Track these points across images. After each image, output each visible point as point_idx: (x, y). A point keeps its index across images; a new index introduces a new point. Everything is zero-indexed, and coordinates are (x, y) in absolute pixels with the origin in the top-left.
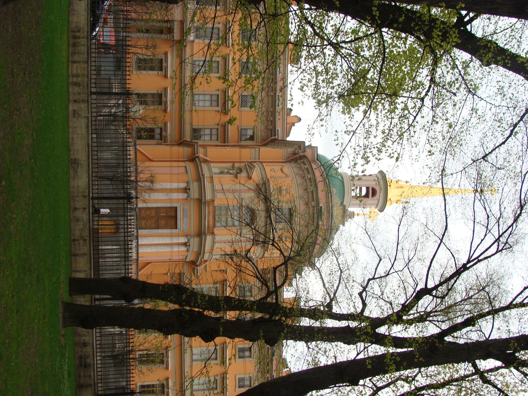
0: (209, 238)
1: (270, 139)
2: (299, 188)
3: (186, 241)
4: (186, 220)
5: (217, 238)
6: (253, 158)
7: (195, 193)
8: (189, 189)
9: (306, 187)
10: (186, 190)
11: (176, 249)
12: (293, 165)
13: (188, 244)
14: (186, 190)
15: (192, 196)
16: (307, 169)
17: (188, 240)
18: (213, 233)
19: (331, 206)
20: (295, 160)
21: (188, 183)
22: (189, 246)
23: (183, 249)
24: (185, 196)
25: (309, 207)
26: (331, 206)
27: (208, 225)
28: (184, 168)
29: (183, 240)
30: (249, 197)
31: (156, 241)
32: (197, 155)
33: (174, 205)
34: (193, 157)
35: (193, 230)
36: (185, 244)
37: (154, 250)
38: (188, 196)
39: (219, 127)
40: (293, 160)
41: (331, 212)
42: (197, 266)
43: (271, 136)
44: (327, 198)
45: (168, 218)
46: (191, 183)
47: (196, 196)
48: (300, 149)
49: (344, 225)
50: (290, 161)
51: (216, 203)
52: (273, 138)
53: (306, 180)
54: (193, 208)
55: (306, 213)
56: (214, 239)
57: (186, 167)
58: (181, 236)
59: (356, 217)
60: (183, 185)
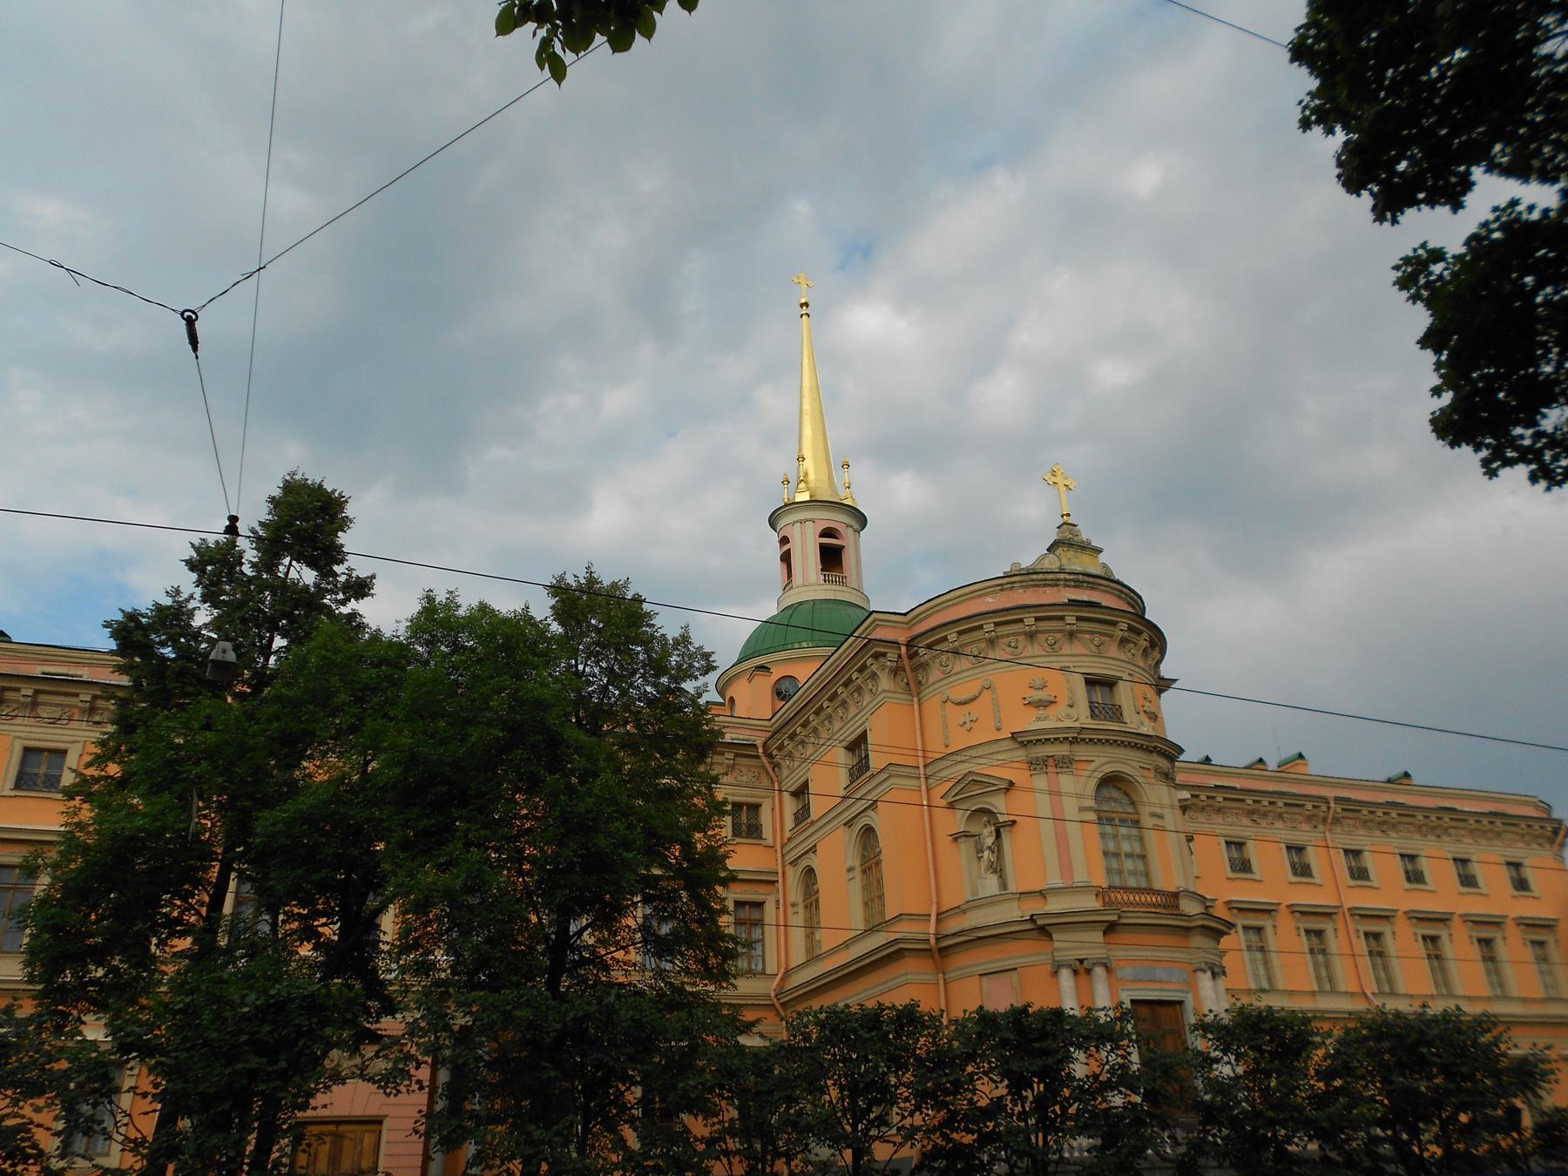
6: (914, 782)
8: (1081, 961)
10: (1082, 969)
12: (935, 674)
15: (1099, 953)
18: (1176, 895)
28: (985, 979)
32: (933, 941)
46: (1059, 956)
48: (884, 655)
49: (1099, 551)
60: (1066, 976)
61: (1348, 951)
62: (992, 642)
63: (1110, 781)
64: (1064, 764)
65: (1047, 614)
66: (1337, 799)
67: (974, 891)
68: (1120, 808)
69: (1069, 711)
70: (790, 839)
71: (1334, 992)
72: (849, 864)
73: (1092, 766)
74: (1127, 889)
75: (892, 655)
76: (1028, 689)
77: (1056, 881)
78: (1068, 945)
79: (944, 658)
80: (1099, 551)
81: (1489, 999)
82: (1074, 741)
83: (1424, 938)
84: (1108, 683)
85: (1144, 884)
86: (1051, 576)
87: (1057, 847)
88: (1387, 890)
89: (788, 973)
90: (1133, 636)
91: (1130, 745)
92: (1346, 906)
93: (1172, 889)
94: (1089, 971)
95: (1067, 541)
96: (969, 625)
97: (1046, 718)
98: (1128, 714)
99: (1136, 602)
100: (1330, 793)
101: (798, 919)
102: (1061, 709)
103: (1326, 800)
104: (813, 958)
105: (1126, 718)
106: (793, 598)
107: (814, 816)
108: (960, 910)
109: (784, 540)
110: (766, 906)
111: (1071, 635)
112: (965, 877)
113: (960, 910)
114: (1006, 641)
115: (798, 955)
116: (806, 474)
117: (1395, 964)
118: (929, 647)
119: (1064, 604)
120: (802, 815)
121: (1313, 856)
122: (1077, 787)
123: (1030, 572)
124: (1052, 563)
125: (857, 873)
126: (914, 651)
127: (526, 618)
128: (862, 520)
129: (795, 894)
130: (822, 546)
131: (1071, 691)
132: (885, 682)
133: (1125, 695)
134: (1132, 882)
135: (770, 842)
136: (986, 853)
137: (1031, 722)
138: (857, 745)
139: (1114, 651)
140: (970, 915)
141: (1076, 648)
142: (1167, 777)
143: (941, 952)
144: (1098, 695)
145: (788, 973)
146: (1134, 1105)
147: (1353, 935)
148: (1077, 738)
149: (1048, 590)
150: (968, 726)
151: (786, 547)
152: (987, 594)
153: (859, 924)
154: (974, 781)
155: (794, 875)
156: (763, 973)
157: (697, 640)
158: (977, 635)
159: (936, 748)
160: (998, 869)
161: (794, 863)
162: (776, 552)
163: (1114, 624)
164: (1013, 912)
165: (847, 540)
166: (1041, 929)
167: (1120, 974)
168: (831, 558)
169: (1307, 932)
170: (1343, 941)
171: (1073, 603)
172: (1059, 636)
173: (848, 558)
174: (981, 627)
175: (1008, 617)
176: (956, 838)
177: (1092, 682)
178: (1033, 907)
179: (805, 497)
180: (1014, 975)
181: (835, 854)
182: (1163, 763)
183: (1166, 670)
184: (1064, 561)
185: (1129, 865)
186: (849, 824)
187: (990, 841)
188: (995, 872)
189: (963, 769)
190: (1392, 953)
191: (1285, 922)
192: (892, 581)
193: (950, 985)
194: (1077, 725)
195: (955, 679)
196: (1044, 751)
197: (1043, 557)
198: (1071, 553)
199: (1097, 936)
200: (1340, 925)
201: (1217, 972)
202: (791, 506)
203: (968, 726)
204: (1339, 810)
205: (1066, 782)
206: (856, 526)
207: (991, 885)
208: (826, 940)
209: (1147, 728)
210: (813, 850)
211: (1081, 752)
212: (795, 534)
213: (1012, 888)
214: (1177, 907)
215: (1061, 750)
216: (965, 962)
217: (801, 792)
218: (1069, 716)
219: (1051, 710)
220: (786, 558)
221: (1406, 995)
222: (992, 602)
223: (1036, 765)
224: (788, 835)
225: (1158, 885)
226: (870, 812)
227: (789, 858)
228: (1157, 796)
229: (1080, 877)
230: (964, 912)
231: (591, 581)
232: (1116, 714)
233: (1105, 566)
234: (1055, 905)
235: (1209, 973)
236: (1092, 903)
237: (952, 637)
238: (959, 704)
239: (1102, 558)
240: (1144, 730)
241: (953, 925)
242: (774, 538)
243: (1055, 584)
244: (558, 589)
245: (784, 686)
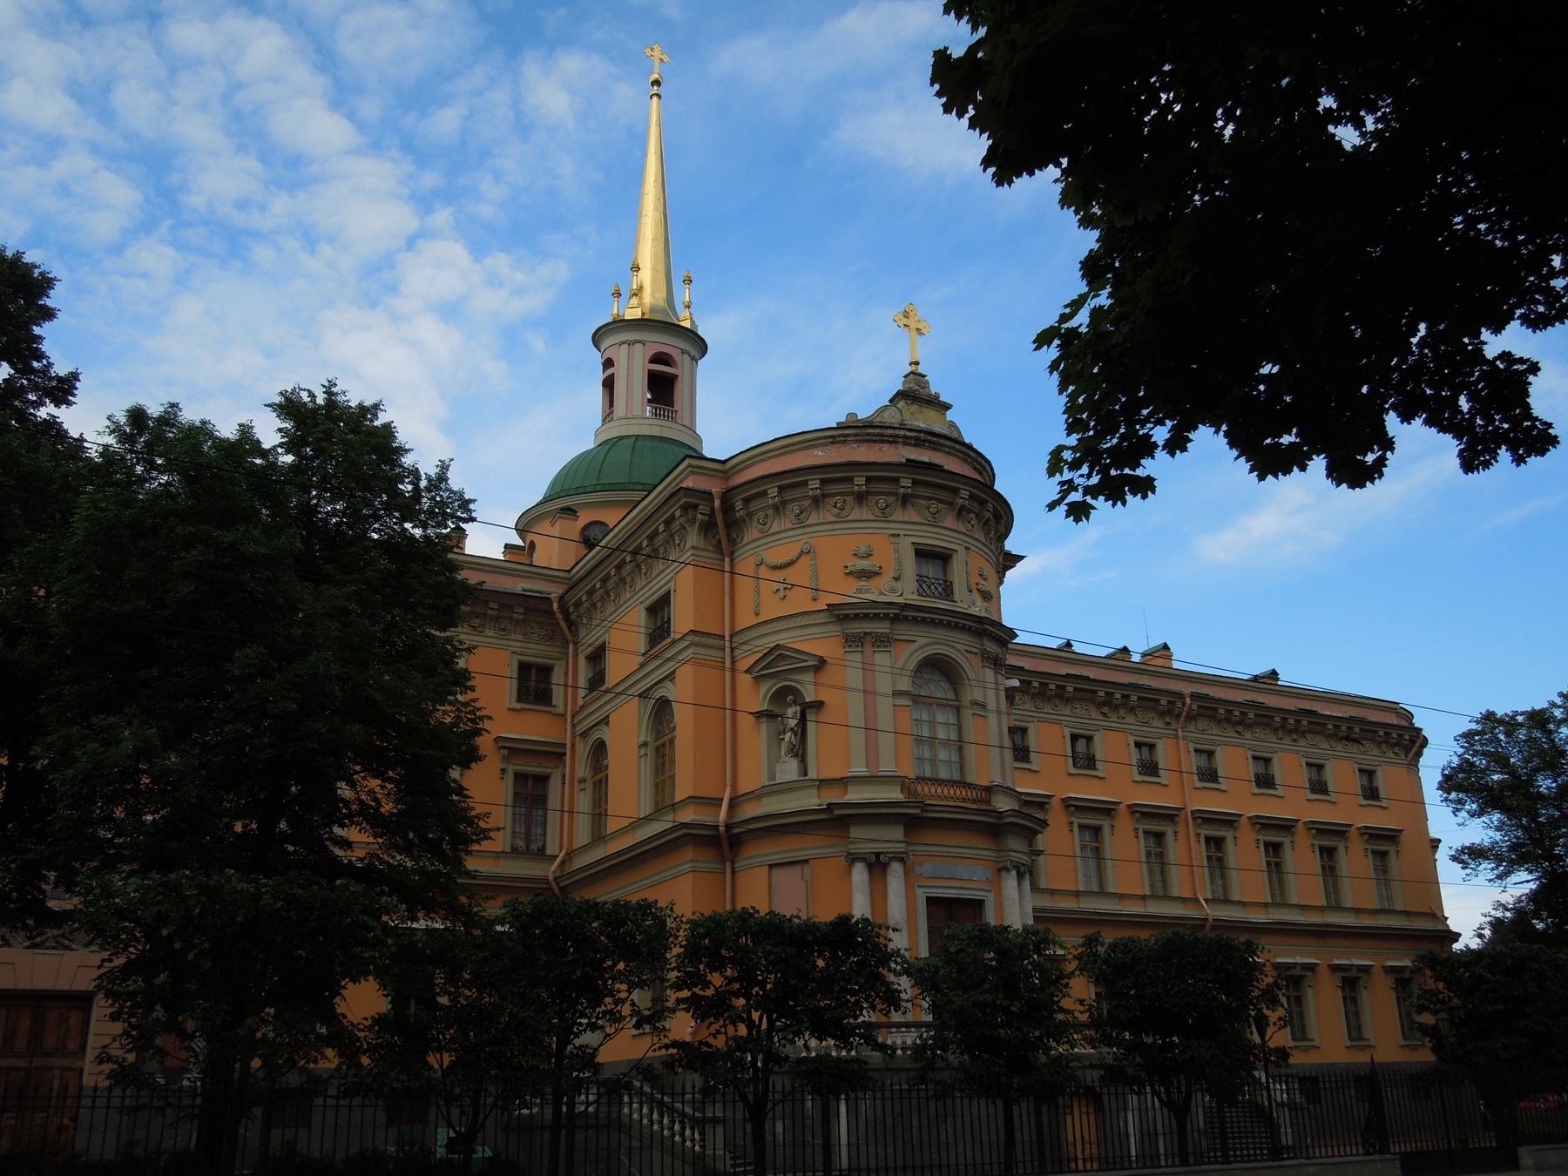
2: (773, 530)
6: (719, 653)
7: (889, 838)
8: (878, 855)
10: (877, 866)
12: (751, 533)
15: (901, 847)
16: (781, 489)
18: (989, 790)
21: (853, 859)
24: (896, 869)
25: (913, 496)
27: (974, 801)
28: (776, 873)
30: (892, 667)
32: (722, 829)
35: (978, 846)
39: (511, 768)
44: (882, 442)
47: (897, 832)
48: (695, 507)
49: (947, 407)
50: (733, 542)
51: (909, 771)
52: (555, 606)
55: (928, 508)
57: (771, 866)
58: (1000, 887)
59: (921, 369)
60: (859, 874)
61: (1186, 862)
63: (938, 666)
64: (883, 641)
65: (881, 476)
66: (1194, 696)
67: (772, 776)
68: (941, 690)
69: (894, 584)
70: (582, 707)
71: (1167, 897)
72: (642, 739)
73: (914, 646)
74: (937, 781)
75: (703, 508)
76: (868, 552)
77: (859, 769)
78: (866, 838)
80: (947, 407)
81: (1322, 909)
82: (895, 619)
83: (1321, 849)
84: (942, 558)
85: (956, 777)
86: (889, 432)
87: (869, 730)
88: (1235, 796)
89: (570, 855)
90: (976, 507)
91: (956, 627)
92: (1190, 809)
93: (986, 783)
94: (885, 866)
95: (915, 393)
96: (790, 482)
97: (868, 591)
98: (959, 591)
99: (982, 465)
100: (1187, 689)
101: (584, 802)
102: (884, 582)
103: (1181, 696)
104: (599, 837)
105: (957, 596)
106: (614, 431)
107: (610, 680)
108: (756, 795)
109: (608, 363)
110: (552, 780)
111: (905, 500)
112: (760, 762)
113: (756, 795)
114: (873, 499)
115: (583, 835)
116: (641, 288)
117: (1233, 875)
118: (747, 501)
119: (901, 464)
120: (597, 681)
121: (1163, 757)
122: (892, 667)
123: (868, 424)
124: (892, 417)
125: (650, 751)
126: (726, 506)
127: (246, 441)
128: (702, 347)
129: (582, 770)
130: (651, 374)
131: (899, 562)
132: (693, 538)
133: (958, 572)
134: (944, 774)
135: (560, 710)
136: (788, 736)
137: (850, 592)
138: (659, 608)
139: (950, 522)
140: (765, 801)
141: (910, 514)
142: (997, 663)
143: (725, 843)
144: (932, 570)
145: (570, 855)
146: (708, 966)
147: (1193, 838)
148: (902, 615)
149: (885, 447)
150: (782, 593)
151: (609, 372)
152: (816, 446)
153: (646, 809)
154: (777, 654)
155: (583, 750)
156: (542, 850)
157: (455, 482)
158: (798, 493)
159: (745, 619)
160: (799, 751)
161: (584, 735)
162: (600, 376)
163: (955, 491)
164: (811, 800)
165: (681, 369)
166: (837, 820)
167: (918, 870)
168: (663, 388)
169: (1082, 827)
170: (1184, 848)
171: (912, 464)
172: (891, 499)
173: (680, 389)
174: (805, 483)
175: (836, 475)
176: (759, 715)
177: (922, 553)
178: (832, 796)
179: (635, 314)
180: (807, 869)
181: (626, 728)
182: (991, 647)
183: (1011, 545)
184: (906, 415)
185: (942, 755)
186: (643, 695)
187: (792, 723)
188: (796, 756)
189: (770, 642)
190: (1232, 865)
191: (1124, 822)
192: (729, 418)
193: (738, 875)
194: (900, 600)
195: (769, 543)
196: (863, 624)
197: (883, 409)
198: (914, 408)
200: (1181, 828)
201: (1026, 872)
202: (619, 324)
203: (782, 593)
204: (1194, 707)
205: (882, 659)
206: (694, 352)
207: (789, 770)
208: (612, 825)
209: (978, 609)
210: (605, 721)
211: (903, 631)
212: (621, 356)
213: (812, 774)
214: (989, 802)
215: (882, 628)
216: (758, 854)
217: (597, 656)
218: (893, 590)
219: (875, 581)
220: (609, 384)
221: (1239, 903)
222: (820, 456)
223: (852, 641)
224: (580, 702)
225: (971, 778)
226: (668, 684)
227: (580, 729)
228: (985, 686)
229: (887, 766)
230: (760, 797)
231: (331, 402)
232: (948, 592)
233: (952, 425)
234: (855, 795)
235: (1014, 873)
236: (895, 794)
238: (775, 568)
239: (950, 415)
240: (975, 611)
241: (750, 811)
242: (597, 358)
243: (893, 440)
244: (289, 407)
245: (594, 533)
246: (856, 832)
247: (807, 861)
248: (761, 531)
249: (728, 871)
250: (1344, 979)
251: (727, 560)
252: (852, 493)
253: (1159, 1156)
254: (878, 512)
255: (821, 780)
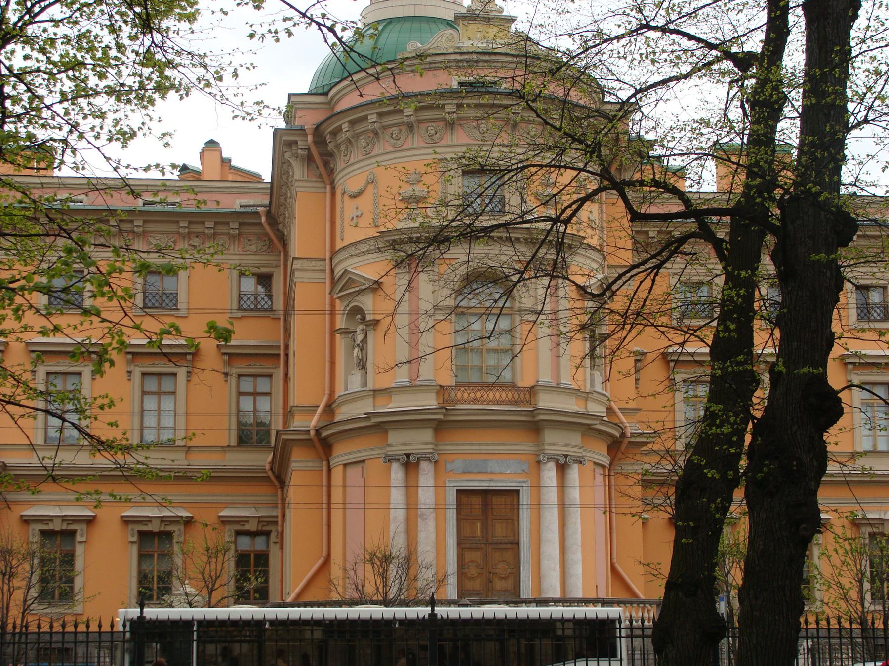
0: (545, 401)
1: (268, 229)
3: (552, 465)
4: (493, 466)
5: (545, 378)
6: (321, 275)
7: (419, 441)
8: (408, 455)
9: (404, 128)
10: (410, 464)
11: (575, 494)
12: (340, 164)
13: (562, 461)
14: (410, 464)
15: (429, 448)
16: (352, 123)
17: (549, 460)
18: (532, 390)
19: (458, 57)
20: (328, 158)
21: (390, 460)
22: (566, 456)
23: (574, 474)
24: (425, 466)
25: (460, 119)
26: (458, 57)
27: (510, 403)
29: (550, 474)
31: (551, 549)
32: (312, 433)
33: (452, 497)
34: (317, 444)
36: (562, 468)
37: (576, 556)
38: (428, 459)
39: (234, 371)
40: (326, 164)
41: (475, 57)
42: (623, 435)
43: (260, 224)
45: (488, 518)
46: (391, 451)
48: (296, 142)
50: (331, 172)
51: (447, 379)
52: (263, 219)
53: (385, 128)
54: (462, 447)
55: (478, 127)
56: (548, 388)
57: (345, 465)
60: (397, 473)
62: (411, 127)
79: (395, 130)
94: (417, 464)
114: (423, 126)
140: (395, 397)
172: (442, 124)
174: (365, 118)
193: (333, 471)
199: (427, 435)
237: (373, 118)
241: (344, 413)
246: (394, 437)
247: (364, 461)
248: (394, 146)
249: (325, 468)
250: (141, 533)
251: (328, 187)
252: (403, 124)
253: (198, 641)
254: (428, 140)
255: (375, 391)
